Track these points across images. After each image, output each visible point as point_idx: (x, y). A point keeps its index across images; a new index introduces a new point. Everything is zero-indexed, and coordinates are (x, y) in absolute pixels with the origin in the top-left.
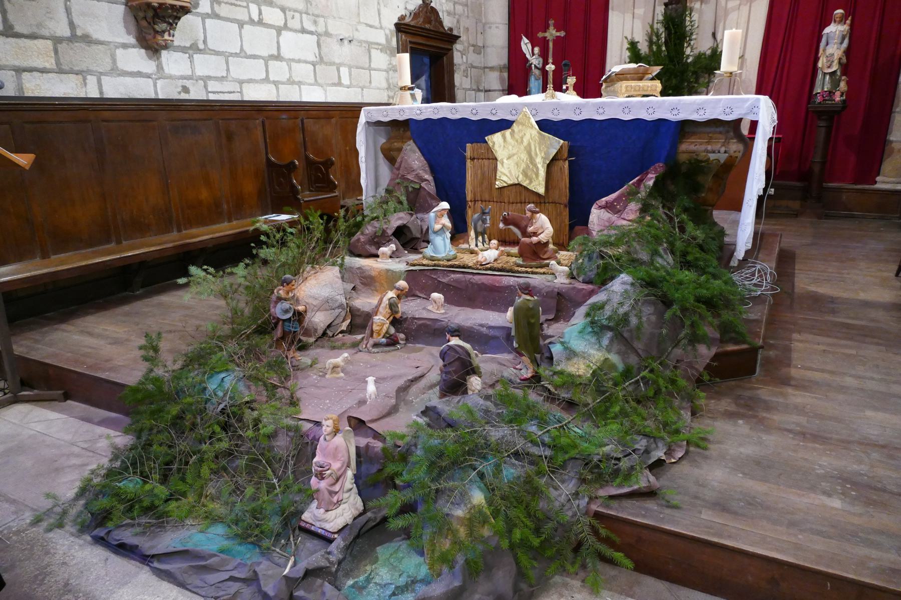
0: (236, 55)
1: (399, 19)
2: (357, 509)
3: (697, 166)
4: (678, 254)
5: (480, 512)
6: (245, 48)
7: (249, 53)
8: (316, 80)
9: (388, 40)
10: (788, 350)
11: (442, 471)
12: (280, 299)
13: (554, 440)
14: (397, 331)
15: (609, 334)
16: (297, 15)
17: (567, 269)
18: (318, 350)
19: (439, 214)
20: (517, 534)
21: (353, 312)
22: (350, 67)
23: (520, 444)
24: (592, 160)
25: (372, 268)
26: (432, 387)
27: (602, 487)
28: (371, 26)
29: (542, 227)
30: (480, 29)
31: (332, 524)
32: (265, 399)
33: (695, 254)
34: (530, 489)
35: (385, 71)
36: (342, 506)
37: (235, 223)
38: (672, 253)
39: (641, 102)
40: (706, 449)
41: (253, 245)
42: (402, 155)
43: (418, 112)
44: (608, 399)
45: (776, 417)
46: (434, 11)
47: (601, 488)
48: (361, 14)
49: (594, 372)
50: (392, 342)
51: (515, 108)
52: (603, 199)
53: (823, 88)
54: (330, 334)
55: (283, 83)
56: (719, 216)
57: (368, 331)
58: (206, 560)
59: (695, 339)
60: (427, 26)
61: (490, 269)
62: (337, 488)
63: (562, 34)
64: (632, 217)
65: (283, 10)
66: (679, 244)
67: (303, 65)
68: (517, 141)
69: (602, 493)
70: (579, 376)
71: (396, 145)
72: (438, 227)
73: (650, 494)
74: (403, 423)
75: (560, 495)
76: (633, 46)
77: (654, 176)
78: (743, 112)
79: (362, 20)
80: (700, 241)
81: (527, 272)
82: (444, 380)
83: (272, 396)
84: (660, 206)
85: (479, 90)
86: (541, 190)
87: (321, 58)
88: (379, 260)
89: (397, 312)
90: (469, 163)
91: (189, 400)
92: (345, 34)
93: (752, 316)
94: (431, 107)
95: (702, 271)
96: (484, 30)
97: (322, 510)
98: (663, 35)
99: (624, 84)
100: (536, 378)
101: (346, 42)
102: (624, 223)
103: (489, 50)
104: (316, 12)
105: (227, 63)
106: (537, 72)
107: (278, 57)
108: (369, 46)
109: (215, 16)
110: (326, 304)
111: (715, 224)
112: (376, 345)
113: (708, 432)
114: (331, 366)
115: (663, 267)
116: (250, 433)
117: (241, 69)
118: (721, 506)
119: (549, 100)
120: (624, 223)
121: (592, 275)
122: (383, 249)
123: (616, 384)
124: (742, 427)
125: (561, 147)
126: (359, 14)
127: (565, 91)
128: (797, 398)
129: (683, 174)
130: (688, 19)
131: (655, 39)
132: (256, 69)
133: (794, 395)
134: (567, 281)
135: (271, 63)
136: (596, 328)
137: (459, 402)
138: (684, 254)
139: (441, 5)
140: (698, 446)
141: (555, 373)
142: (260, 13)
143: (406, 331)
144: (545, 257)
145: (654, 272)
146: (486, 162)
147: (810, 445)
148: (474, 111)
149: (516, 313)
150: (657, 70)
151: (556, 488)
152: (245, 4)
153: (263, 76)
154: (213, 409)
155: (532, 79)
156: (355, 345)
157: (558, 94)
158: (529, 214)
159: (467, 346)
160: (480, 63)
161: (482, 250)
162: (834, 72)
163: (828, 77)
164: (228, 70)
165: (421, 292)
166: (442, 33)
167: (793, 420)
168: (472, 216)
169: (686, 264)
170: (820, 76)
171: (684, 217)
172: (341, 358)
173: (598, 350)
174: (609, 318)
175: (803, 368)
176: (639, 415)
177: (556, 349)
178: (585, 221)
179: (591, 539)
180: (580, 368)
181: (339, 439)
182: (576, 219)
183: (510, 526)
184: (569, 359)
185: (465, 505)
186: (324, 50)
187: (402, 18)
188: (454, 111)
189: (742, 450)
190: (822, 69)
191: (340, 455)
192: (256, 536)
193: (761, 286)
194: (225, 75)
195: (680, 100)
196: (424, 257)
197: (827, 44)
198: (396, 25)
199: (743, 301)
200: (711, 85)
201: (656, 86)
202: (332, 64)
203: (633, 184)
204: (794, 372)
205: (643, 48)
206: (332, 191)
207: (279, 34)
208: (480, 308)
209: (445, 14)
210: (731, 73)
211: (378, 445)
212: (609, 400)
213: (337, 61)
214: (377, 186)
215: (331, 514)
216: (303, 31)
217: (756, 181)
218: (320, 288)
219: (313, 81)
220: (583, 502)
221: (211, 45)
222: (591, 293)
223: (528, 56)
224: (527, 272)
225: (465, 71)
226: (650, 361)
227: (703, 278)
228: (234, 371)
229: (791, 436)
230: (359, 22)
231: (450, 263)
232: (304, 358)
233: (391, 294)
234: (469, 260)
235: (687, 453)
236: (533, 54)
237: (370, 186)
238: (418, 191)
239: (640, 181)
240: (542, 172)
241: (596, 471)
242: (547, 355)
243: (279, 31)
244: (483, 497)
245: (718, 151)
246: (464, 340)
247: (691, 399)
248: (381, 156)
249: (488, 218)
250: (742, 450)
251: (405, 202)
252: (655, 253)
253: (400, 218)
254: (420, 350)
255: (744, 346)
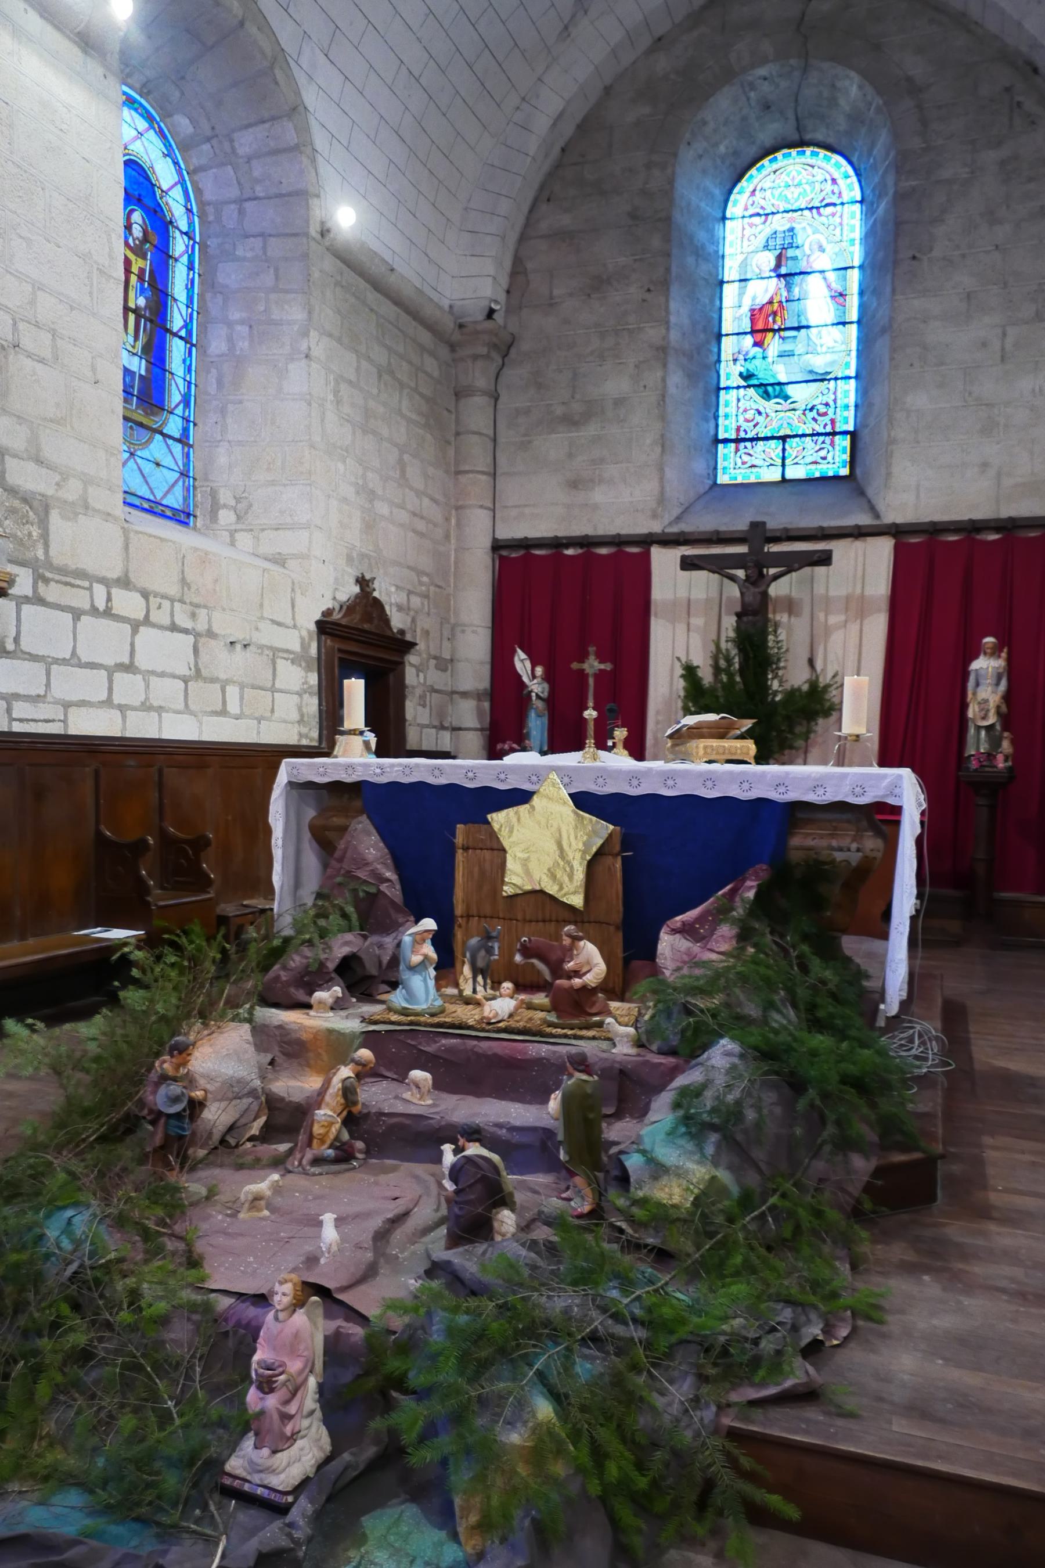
0: (64, 662)
1: (324, 614)
2: (321, 1448)
3: (818, 871)
4: (802, 1007)
5: (550, 1433)
6: (79, 651)
7: (84, 659)
8: (186, 705)
9: (305, 647)
10: (978, 1162)
11: (484, 1365)
12: (164, 1078)
13: (649, 1310)
14: (352, 1136)
15: (714, 1137)
16: (166, 604)
17: (631, 1030)
18: (217, 1171)
19: (418, 937)
20: (613, 1470)
21: (273, 1104)
22: (242, 687)
23: (598, 1321)
24: (657, 856)
25: (303, 1028)
26: (427, 1230)
27: (734, 1387)
28: (279, 624)
29: (588, 963)
30: (446, 633)
31: (282, 1476)
32: (140, 1257)
33: (827, 1008)
34: (621, 1398)
35: (297, 693)
36: (300, 1443)
37: (31, 941)
38: (794, 1006)
39: (731, 773)
40: (881, 1322)
41: (116, 983)
42: (347, 837)
43: (378, 771)
44: (722, 1244)
45: (978, 1269)
46: (377, 604)
47: (733, 1389)
48: (266, 603)
49: (695, 1199)
50: (344, 1156)
51: (538, 774)
52: (678, 918)
53: (978, 748)
54: (233, 1142)
55: (134, 709)
56: (851, 945)
57: (302, 1137)
58: (61, 1554)
59: (846, 1144)
60: (366, 626)
61: (505, 1030)
62: (292, 1409)
63: (607, 666)
64: (724, 947)
65: (145, 595)
66: (801, 992)
67: (168, 681)
68: (539, 823)
69: (734, 1397)
70: (674, 1206)
71: (337, 821)
72: (416, 959)
73: (807, 1396)
74: (390, 1294)
75: (670, 1404)
76: (690, 672)
77: (755, 883)
78: (881, 793)
79: (265, 615)
80: (831, 986)
81: (566, 1036)
82: (457, 1217)
83: (155, 1252)
84: (767, 930)
85: (443, 728)
86: (577, 901)
87: (198, 671)
88: (312, 1013)
89: (355, 1103)
90: (460, 856)
91: (14, 1257)
92: (238, 635)
93: (922, 1108)
94: (400, 765)
95: (841, 1035)
96: (453, 634)
97: (266, 1451)
98: (737, 660)
99: (702, 743)
100: (596, 1214)
101: (238, 647)
102: (714, 956)
103: (461, 666)
104: (196, 600)
105: (48, 674)
106: (540, 704)
107: (129, 668)
108: (275, 653)
109: (38, 600)
110: (233, 1091)
111: (849, 960)
112: (317, 1161)
113: (881, 1296)
114: (250, 1197)
115: (785, 1028)
116: (125, 1316)
117: (69, 684)
118: (919, 1410)
119: (588, 763)
120: (714, 956)
121: (675, 1040)
122: (319, 995)
123: (731, 1220)
124: (929, 1286)
125: (610, 835)
126: (261, 605)
127: (609, 749)
128: (1005, 1237)
129: (795, 879)
130: (771, 637)
131: (723, 663)
132: (94, 686)
133: (999, 1234)
134: (633, 1051)
135: (118, 676)
136: (692, 1126)
137: (484, 1253)
138: (812, 1008)
139: (389, 594)
140: (869, 1318)
141: (636, 1202)
142: (109, 599)
143: (374, 1138)
144: (594, 1010)
145: (771, 1036)
146: (487, 854)
147: (1033, 1310)
148: (470, 775)
149: (566, 1102)
150: (748, 724)
151: (662, 1393)
152: (86, 584)
153: (104, 696)
154: (56, 1275)
155: (532, 715)
156: (278, 1163)
157: (602, 753)
158: (567, 941)
159: (495, 1158)
160: (446, 684)
161: (488, 999)
162: (992, 726)
163: (983, 733)
164: (48, 685)
165: (389, 1070)
166: (389, 638)
167: (1003, 1273)
168: (466, 940)
169: (816, 1024)
170: (972, 731)
171: (805, 948)
172: (265, 1184)
173: (699, 1163)
174: (714, 1110)
175: (1006, 1190)
176: (773, 1269)
177: (633, 1162)
178: (650, 952)
179: (726, 1478)
180: (673, 1193)
181: (300, 1318)
182: (634, 951)
183: (599, 1455)
184: (655, 1178)
185: (525, 1423)
186: (204, 657)
187: (328, 613)
188: (437, 772)
189: (935, 1322)
190: (973, 720)
191: (302, 1347)
192: (150, 1503)
193: (926, 1059)
194: (42, 693)
195: (787, 773)
196: (390, 1009)
197: (977, 685)
198: (319, 623)
199: (906, 1083)
200: (812, 736)
201: (748, 748)
202: (213, 680)
203: (723, 895)
204: (993, 1198)
205: (706, 675)
206: (204, 891)
207: (135, 631)
208: (490, 1096)
209: (394, 609)
210: (858, 736)
211: (356, 1331)
212: (725, 1246)
213: (223, 676)
214: (297, 884)
215: (282, 1457)
216: (174, 628)
217: (905, 899)
218: (221, 1057)
219: (181, 706)
220: (709, 1414)
221: (25, 645)
222: (674, 1072)
223: (525, 679)
224: (566, 1036)
225: (423, 697)
226: (780, 1180)
227: (844, 1045)
228: (88, 1206)
229: (1005, 1297)
230: (262, 618)
231: (436, 1020)
232: (194, 1186)
233: (346, 1072)
234: (468, 1015)
235: (854, 1330)
236: (534, 677)
237: (286, 888)
238: (374, 897)
239: (733, 892)
240: (580, 875)
241: (725, 1362)
242: (615, 1172)
243: (136, 626)
244: (550, 1409)
245: (849, 849)
246: (490, 1150)
247: (846, 1241)
248: (307, 835)
249: (496, 946)
250: (935, 1322)
251: (354, 917)
252: (769, 1005)
253: (347, 943)
254: (394, 1169)
255: (917, 1155)
